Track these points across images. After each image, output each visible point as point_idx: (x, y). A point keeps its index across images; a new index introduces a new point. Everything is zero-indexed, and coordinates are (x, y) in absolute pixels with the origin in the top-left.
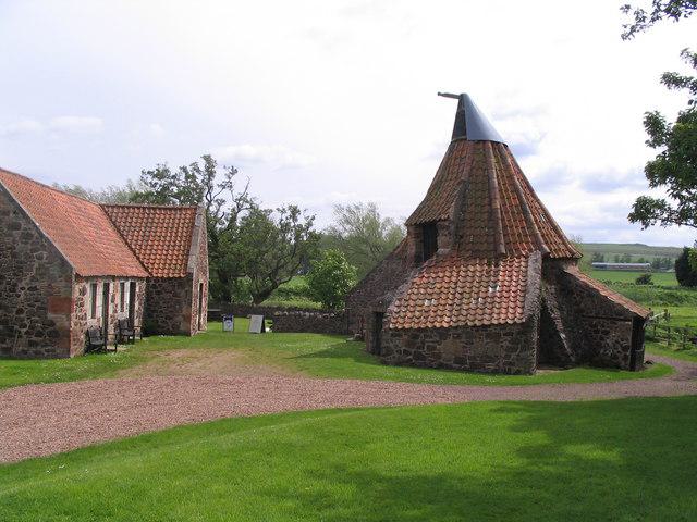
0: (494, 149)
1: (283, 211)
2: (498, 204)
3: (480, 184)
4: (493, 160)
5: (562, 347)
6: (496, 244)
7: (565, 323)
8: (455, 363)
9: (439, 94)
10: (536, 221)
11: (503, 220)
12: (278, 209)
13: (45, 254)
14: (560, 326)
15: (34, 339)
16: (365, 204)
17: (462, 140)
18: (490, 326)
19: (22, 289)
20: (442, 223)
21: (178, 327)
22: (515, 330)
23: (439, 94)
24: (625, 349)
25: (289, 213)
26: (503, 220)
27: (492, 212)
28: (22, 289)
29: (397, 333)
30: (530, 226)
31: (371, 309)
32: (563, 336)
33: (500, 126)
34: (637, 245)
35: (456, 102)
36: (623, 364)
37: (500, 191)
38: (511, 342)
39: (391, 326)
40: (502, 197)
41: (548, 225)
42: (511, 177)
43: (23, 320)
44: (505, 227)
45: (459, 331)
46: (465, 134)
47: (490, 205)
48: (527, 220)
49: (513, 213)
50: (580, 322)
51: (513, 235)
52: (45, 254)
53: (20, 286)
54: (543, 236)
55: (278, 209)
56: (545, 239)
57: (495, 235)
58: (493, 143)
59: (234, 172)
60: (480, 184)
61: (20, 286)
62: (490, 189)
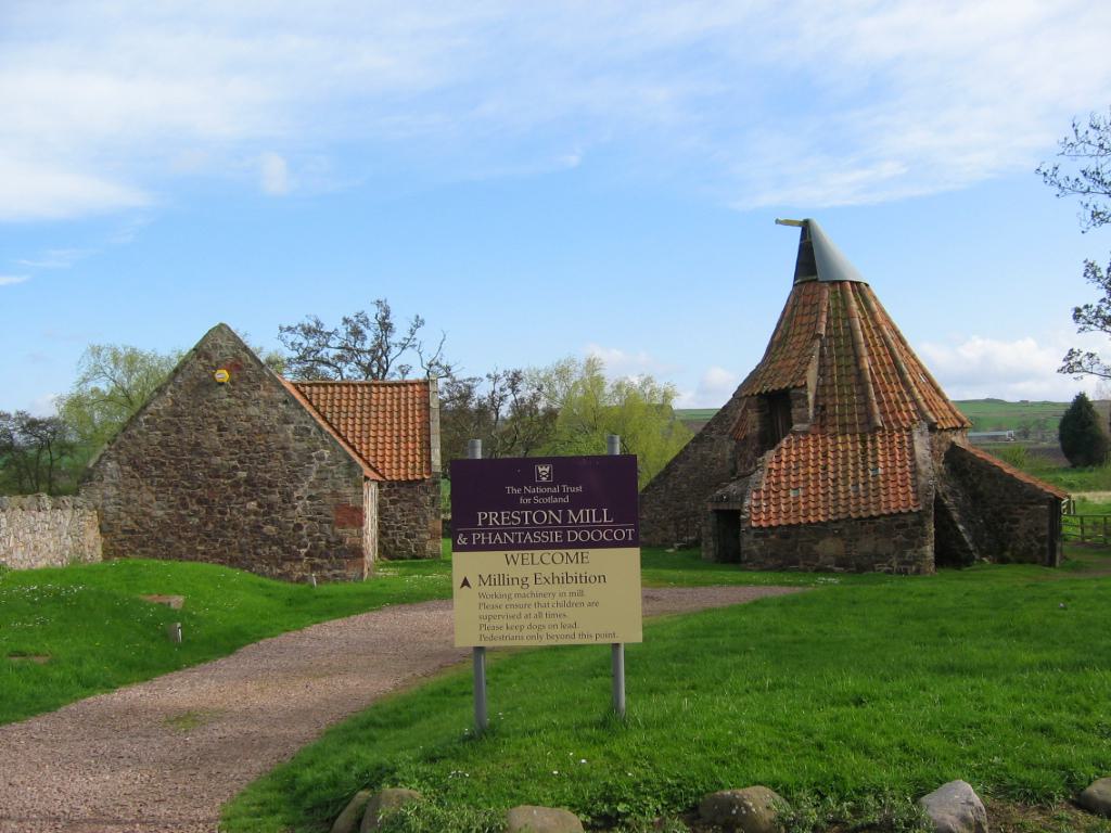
0: (854, 291)
1: (496, 379)
2: (866, 363)
3: (830, 332)
4: (854, 305)
5: (962, 542)
6: (869, 415)
7: (962, 511)
8: (837, 566)
9: (777, 222)
10: (915, 383)
11: (874, 383)
12: (489, 376)
13: (327, 453)
14: (956, 515)
15: (317, 560)
16: (581, 359)
17: (810, 281)
18: (878, 517)
19: (299, 498)
20: (798, 391)
21: (424, 548)
22: (910, 520)
23: (777, 222)
24: (1041, 540)
25: (503, 382)
26: (874, 383)
27: (860, 373)
28: (299, 498)
29: (762, 532)
30: (910, 392)
31: (710, 508)
32: (961, 527)
33: (851, 258)
34: (988, 401)
35: (798, 231)
36: (1039, 558)
37: (868, 346)
38: (907, 535)
39: (754, 524)
40: (871, 355)
41: (929, 386)
42: (878, 327)
43: (301, 537)
44: (877, 393)
45: (840, 527)
46: (815, 273)
47: (857, 365)
48: (905, 383)
49: (886, 374)
50: (992, 505)
51: (889, 401)
52: (327, 453)
53: (296, 495)
54: (925, 401)
55: (489, 376)
56: (928, 406)
57: (866, 402)
58: (852, 282)
59: (419, 323)
60: (830, 332)
61: (296, 495)
62: (854, 345)
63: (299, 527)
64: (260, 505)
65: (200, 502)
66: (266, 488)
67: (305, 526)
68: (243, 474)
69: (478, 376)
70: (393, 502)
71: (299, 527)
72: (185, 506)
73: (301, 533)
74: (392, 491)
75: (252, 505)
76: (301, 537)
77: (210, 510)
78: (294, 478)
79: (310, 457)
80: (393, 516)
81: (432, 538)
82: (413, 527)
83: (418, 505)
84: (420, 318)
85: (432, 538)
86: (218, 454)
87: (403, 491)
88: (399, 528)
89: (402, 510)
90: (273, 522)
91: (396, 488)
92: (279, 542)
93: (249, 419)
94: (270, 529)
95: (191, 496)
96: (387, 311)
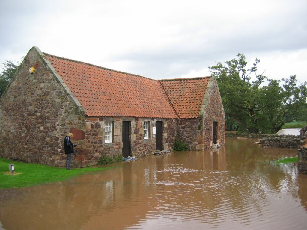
12: (283, 79)
28: (58, 125)
53: (57, 123)
63: (57, 139)
64: (45, 128)
65: (26, 126)
66: (47, 120)
67: (60, 138)
68: (38, 114)
69: (248, 71)
70: (183, 128)
71: (57, 139)
72: (21, 128)
73: (58, 141)
74: (182, 123)
75: (42, 128)
76: (58, 144)
77: (29, 130)
78: (56, 115)
79: (62, 106)
80: (183, 134)
81: (199, 144)
82: (191, 139)
83: (194, 130)
84: (238, 55)
85: (199, 144)
86: (31, 105)
87: (187, 123)
88: (185, 139)
89: (186, 131)
90: (49, 136)
91: (184, 122)
92: (51, 146)
93: (41, 89)
94: (47, 139)
95: (23, 124)
96: (243, 58)
